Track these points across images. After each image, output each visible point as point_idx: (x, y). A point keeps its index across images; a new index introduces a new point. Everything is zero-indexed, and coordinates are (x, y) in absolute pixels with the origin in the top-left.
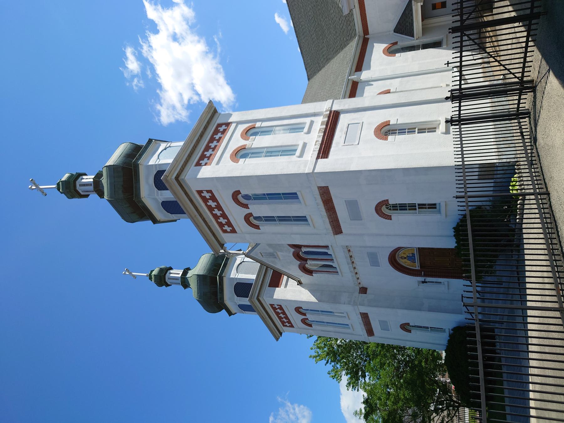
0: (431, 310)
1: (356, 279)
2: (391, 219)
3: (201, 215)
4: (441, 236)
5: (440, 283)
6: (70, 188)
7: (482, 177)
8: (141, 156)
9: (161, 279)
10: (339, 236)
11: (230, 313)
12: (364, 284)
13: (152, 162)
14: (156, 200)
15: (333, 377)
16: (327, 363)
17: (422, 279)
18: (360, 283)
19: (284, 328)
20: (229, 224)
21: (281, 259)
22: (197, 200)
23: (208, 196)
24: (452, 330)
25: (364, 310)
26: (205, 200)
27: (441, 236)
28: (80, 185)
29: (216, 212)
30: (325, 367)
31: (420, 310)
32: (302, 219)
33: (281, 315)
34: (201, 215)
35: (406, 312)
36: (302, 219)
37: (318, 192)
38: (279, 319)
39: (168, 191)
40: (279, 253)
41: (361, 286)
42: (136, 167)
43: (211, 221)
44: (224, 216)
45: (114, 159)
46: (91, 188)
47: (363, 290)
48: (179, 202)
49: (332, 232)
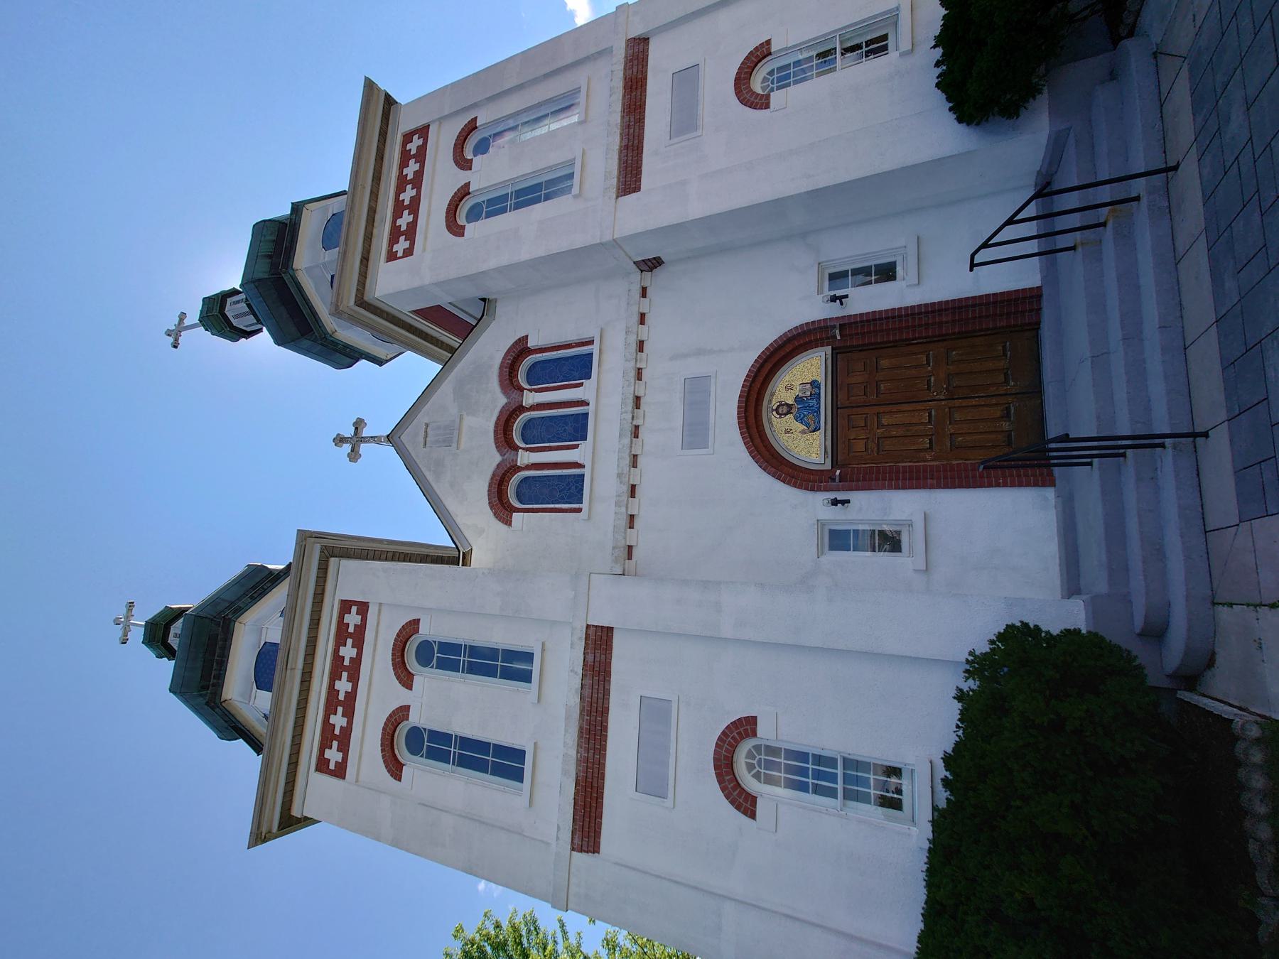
32: (505, 762)
36: (505, 762)
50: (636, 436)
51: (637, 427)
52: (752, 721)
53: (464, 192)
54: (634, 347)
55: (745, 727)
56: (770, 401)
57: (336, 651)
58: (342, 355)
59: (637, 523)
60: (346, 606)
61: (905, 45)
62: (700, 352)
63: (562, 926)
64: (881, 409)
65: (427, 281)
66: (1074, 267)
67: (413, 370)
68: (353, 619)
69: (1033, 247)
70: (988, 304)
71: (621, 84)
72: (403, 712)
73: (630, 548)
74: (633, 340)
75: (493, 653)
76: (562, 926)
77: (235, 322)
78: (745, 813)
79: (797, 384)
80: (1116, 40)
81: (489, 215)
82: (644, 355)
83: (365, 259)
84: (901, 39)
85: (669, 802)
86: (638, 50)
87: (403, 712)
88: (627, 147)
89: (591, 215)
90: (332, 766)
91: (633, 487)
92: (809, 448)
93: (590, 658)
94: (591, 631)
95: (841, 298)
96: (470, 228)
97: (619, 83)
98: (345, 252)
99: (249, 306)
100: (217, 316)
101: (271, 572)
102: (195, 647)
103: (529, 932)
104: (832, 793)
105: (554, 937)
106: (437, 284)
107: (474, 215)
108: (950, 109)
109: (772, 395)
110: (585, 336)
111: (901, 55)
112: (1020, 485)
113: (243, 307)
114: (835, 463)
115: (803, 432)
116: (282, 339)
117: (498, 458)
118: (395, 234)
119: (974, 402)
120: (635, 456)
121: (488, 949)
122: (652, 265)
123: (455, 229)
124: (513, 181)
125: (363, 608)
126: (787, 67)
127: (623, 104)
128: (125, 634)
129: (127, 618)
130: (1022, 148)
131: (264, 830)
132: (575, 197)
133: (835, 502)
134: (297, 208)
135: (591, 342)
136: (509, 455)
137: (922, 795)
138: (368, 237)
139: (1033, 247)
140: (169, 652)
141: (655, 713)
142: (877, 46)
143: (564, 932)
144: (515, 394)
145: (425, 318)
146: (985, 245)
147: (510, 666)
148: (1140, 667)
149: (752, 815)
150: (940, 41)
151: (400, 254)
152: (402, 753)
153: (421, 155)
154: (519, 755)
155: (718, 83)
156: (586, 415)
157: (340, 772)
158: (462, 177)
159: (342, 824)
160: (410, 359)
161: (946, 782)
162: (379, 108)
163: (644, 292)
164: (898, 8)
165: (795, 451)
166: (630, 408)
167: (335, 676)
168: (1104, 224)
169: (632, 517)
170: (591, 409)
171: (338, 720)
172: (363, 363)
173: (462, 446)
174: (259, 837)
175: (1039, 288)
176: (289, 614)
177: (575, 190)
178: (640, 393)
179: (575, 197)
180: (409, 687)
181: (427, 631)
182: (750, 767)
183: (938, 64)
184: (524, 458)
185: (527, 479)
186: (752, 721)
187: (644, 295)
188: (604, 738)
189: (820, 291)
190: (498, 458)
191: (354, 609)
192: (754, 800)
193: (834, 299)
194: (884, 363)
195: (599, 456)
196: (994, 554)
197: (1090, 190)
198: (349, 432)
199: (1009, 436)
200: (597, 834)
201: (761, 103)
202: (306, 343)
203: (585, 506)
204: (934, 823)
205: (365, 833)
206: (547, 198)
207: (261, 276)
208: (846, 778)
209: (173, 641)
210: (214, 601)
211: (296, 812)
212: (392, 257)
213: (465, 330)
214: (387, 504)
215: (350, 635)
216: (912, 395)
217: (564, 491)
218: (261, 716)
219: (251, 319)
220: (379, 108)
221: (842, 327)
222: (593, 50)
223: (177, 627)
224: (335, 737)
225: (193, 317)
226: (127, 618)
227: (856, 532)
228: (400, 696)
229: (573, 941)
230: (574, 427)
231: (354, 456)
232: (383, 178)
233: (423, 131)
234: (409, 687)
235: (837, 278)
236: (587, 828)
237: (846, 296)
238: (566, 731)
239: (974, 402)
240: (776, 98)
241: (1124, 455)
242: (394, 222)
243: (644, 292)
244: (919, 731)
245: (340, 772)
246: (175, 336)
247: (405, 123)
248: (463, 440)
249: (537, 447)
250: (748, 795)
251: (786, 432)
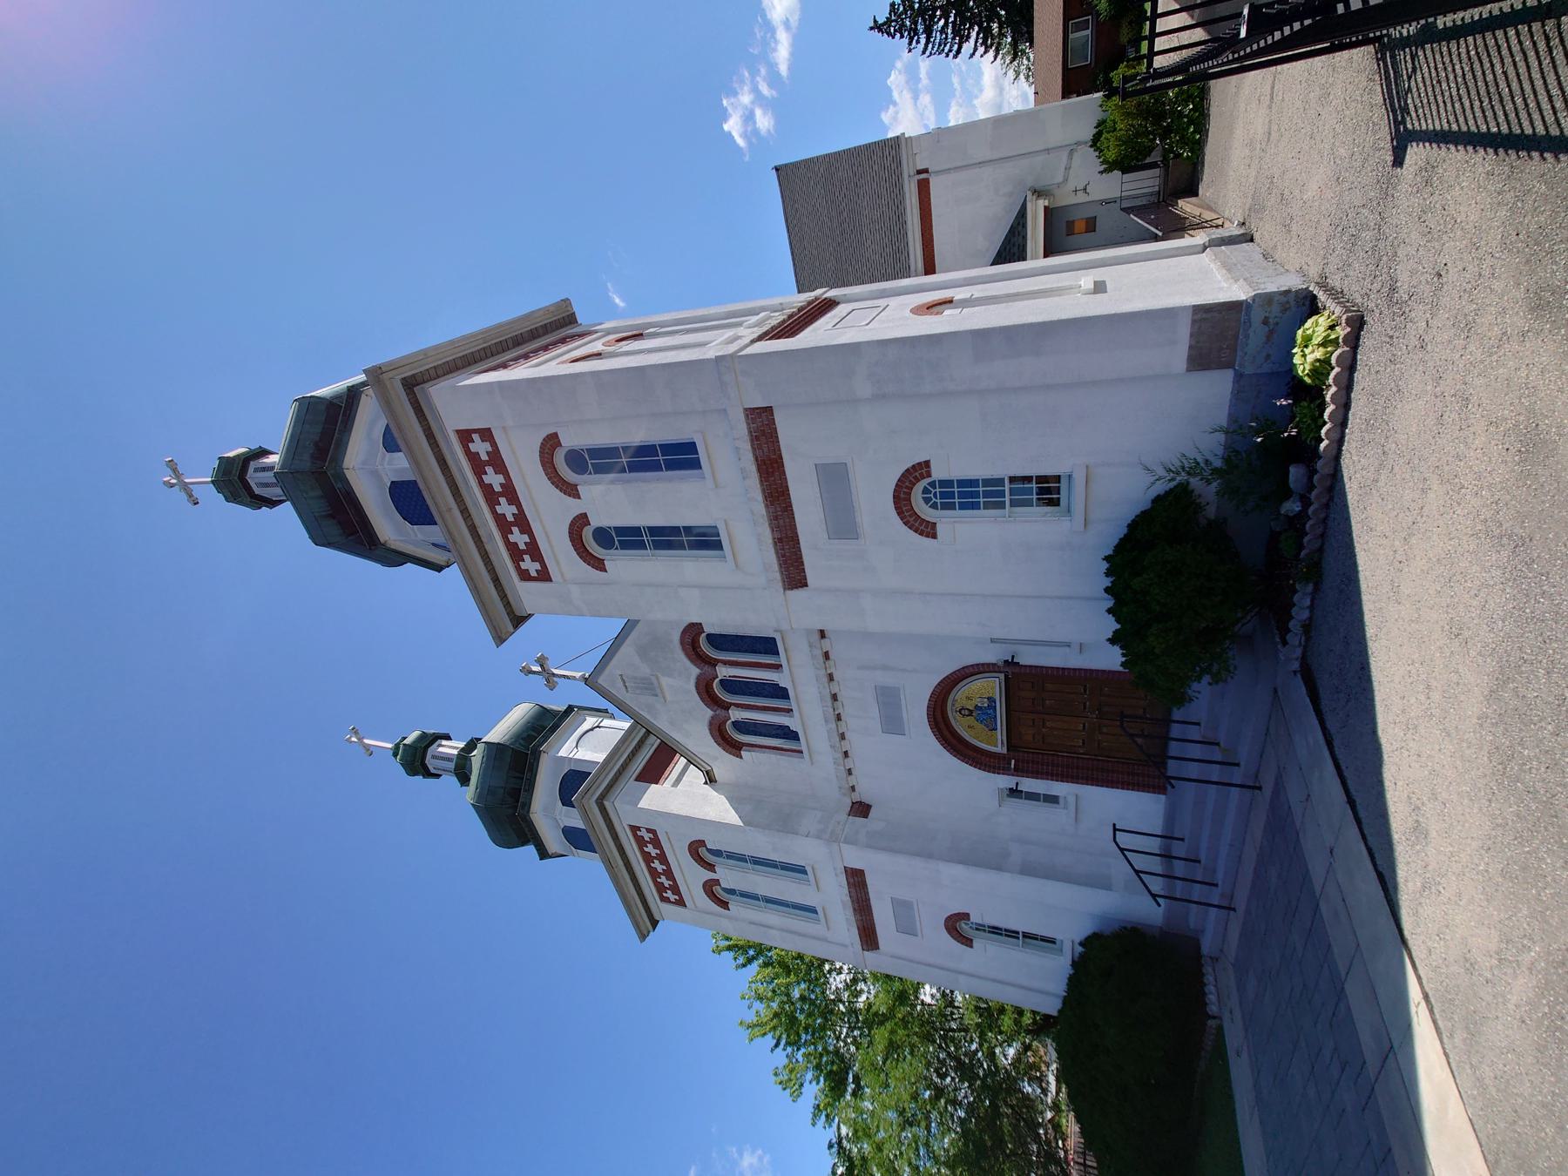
0: (1028, 870)
1: (844, 774)
2: (934, 536)
3: (465, 511)
4: (1070, 598)
5: (1053, 799)
6: (416, 759)
7: (1200, 360)
8: (546, 739)
9: (416, 759)
10: (797, 594)
11: (543, 854)
12: (864, 794)
13: (563, 753)
14: (375, 474)
15: (784, 1085)
16: (777, 1045)
17: (1005, 781)
18: (853, 788)
19: (664, 907)
20: (675, 889)
21: (669, 698)
22: (457, 462)
23: (647, 836)
24: (1081, 944)
25: (856, 859)
26: (641, 842)
27: (1070, 598)
28: (434, 757)
29: (657, 864)
30: (769, 1056)
31: (999, 868)
32: (705, 540)
33: (663, 879)
34: (465, 511)
35: (959, 870)
36: (705, 540)
37: (744, 426)
38: (649, 877)
39: (400, 454)
40: (666, 681)
41: (856, 797)
42: (536, 755)
43: (491, 536)
44: (669, 874)
45: (499, 732)
46: (452, 766)
47: (861, 809)
48: (421, 486)
49: (778, 576)
74: (819, 653)
82: (831, 663)
87: (580, 522)
100: (235, 479)
104: (1001, 505)
147: (682, 456)
149: (934, 536)
154: (691, 447)
155: (873, 496)
157: (544, 576)
171: (494, 479)
181: (569, 440)
182: (927, 500)
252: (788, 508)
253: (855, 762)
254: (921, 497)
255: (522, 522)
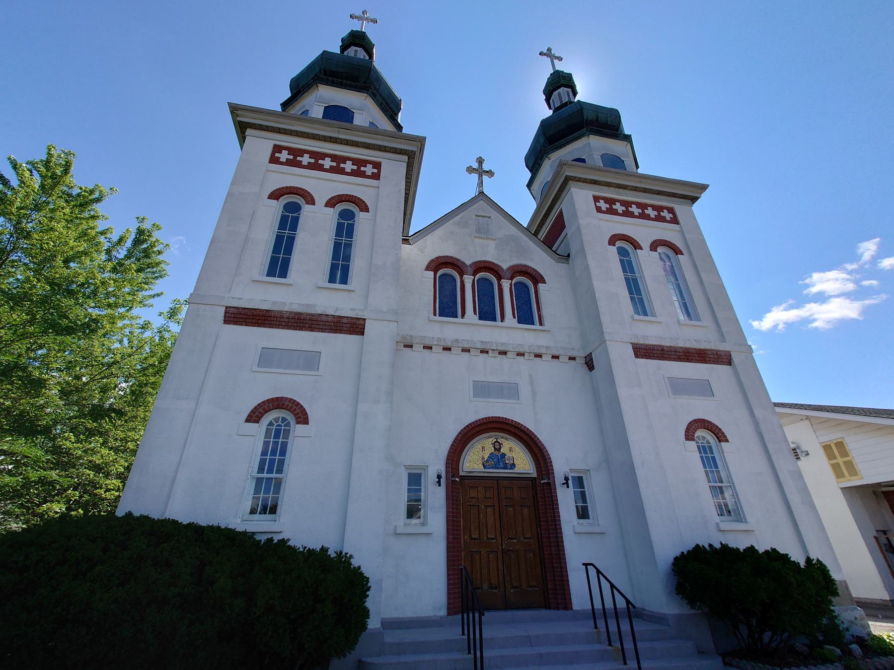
32: (279, 266)
36: (279, 266)
50: (482, 352)
51: (487, 352)
52: (306, 422)
53: (636, 246)
54: (538, 352)
55: (302, 417)
56: (502, 438)
57: (349, 159)
58: (534, 161)
59: (427, 351)
60: (377, 165)
61: (723, 526)
62: (534, 394)
63: (158, 295)
64: (497, 509)
65: (580, 221)
66: (586, 627)
67: (524, 208)
68: (369, 170)
69: (598, 605)
70: (562, 576)
71: (702, 347)
72: (311, 200)
73: (411, 346)
74: (543, 351)
75: (347, 258)
76: (158, 295)
77: (556, 93)
78: (249, 416)
79: (513, 454)
80: (723, 655)
81: (622, 261)
82: (533, 357)
83: (594, 182)
84: (727, 524)
85: (255, 368)
86: (722, 358)
87: (311, 200)
88: (663, 350)
89: (621, 328)
90: (277, 155)
91: (449, 349)
92: (473, 461)
93: (345, 321)
94: (361, 322)
95: (567, 484)
96: (613, 250)
97: (703, 346)
98: (599, 170)
99: (566, 104)
100: (559, 83)
101: (397, 115)
102: (349, 68)
103: (154, 273)
104: (261, 470)
105: (150, 289)
106: (579, 228)
107: (622, 252)
108: (683, 553)
109: (507, 439)
110: (546, 321)
111: (717, 524)
112: (449, 594)
113: (565, 99)
114: (463, 478)
115: (483, 458)
116: (545, 124)
117: (468, 263)
118: (610, 201)
119: (500, 566)
120: (469, 351)
121: (145, 246)
122: (590, 364)
123: (613, 240)
124: (642, 277)
125: (376, 176)
126: (712, 452)
127: (690, 348)
128: (356, 17)
129: (367, 19)
130: (656, 596)
131: (238, 112)
132: (632, 316)
133: (439, 477)
134: (628, 138)
135: (541, 324)
136: (470, 270)
137: (260, 525)
138: (608, 185)
139: (598, 605)
140: (344, 48)
141: (311, 361)
142: (724, 510)
143: (154, 296)
144: (508, 275)
145: (557, 218)
146: (598, 572)
147: (340, 270)
148: (345, 656)
149: (248, 420)
150: (725, 547)
151: (598, 204)
152: (285, 200)
153: (660, 219)
154: (284, 274)
155: (702, 409)
156: (494, 319)
157: (274, 160)
158: (646, 245)
159: (242, 161)
160: (532, 206)
161: (271, 539)
162: (691, 193)
163: (572, 358)
164: (746, 522)
165: (471, 453)
166: (499, 348)
167: (334, 158)
168: (610, 644)
169: (431, 348)
170: (499, 323)
172: (529, 175)
173: (477, 240)
174: (235, 109)
175: (571, 608)
176: (373, 129)
177: (637, 317)
178: (509, 354)
179: (632, 316)
180: (327, 205)
181: (361, 216)
182: (277, 420)
183: (710, 545)
184: (468, 280)
185: (455, 280)
186: (306, 422)
187: (570, 358)
188: (295, 328)
189: (571, 470)
190: (468, 263)
191: (375, 171)
192: (257, 421)
193: (566, 479)
194: (526, 511)
195: (468, 328)
196: (408, 573)
197: (631, 638)
198: (486, 167)
199: (479, 588)
200: (236, 323)
201: (689, 435)
202: (542, 140)
203: (438, 318)
204: (245, 533)
205: (235, 176)
206: (632, 299)
207: (585, 114)
208: (269, 480)
209: (351, 52)
210: (379, 79)
211: (249, 131)
212: (596, 199)
213: (549, 242)
214: (441, 189)
215: (359, 168)
216: (505, 525)
217: (447, 305)
218: (307, 108)
219: (558, 104)
220: (691, 193)
221: (549, 484)
222: (724, 329)
223: (362, 54)
224: (295, 157)
225: (560, 66)
226: (367, 19)
227: (420, 490)
228: (321, 199)
229: (151, 301)
230: (487, 313)
231: (470, 170)
232: (646, 194)
233: (675, 221)
234: (327, 205)
235: (579, 482)
236: (239, 316)
237: (568, 487)
238: (299, 304)
239: (500, 566)
240: (692, 445)
241: (469, 653)
242: (618, 201)
243: (572, 358)
244: (301, 523)
245: (274, 160)
246: (548, 54)
247: (680, 209)
248: (481, 241)
249: (472, 287)
250: (260, 418)
251: (483, 448)
252: (679, 359)
253: (437, 355)
254: (281, 414)
255: (644, 216)
